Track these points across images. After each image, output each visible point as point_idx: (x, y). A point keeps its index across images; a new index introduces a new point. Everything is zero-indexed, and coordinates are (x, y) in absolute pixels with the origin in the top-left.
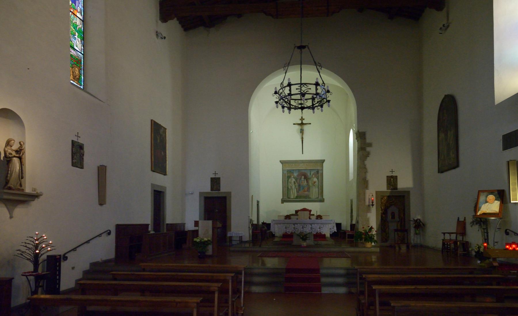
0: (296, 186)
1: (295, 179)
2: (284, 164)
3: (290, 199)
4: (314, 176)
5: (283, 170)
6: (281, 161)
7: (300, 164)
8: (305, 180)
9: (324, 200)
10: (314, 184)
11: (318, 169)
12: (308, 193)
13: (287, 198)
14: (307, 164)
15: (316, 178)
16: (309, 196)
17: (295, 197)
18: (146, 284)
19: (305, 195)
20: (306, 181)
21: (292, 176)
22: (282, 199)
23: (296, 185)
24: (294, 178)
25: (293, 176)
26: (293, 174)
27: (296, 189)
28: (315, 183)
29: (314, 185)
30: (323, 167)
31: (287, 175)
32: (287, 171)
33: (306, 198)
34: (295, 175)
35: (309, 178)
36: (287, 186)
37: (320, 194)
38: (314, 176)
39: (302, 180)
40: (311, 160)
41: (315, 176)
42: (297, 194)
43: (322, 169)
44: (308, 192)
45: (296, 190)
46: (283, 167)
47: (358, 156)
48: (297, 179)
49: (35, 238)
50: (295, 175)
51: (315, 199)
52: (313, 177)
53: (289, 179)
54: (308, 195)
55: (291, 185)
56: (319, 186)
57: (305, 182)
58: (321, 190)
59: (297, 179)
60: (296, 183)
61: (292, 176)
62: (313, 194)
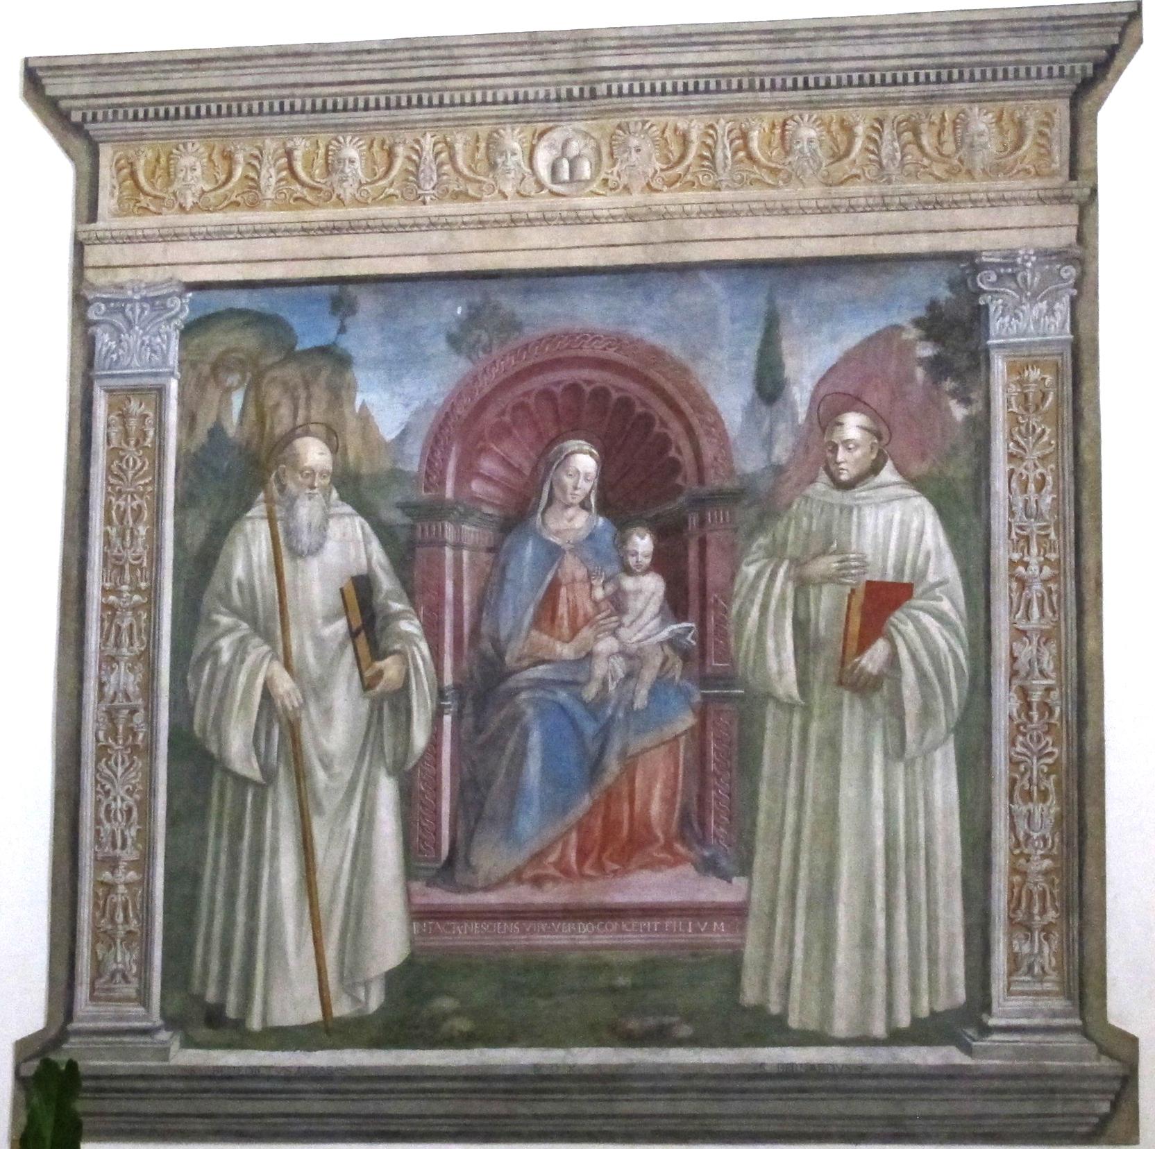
0: (400, 699)
1: (384, 532)
2: (107, 154)
3: (241, 1037)
4: (853, 425)
5: (80, 301)
6: (54, 88)
7: (514, 140)
8: (643, 544)
9: (1127, 1081)
10: (874, 658)
11: (969, 261)
12: (715, 892)
13: (172, 1022)
14: (696, 128)
15: (918, 484)
16: (733, 963)
17: (375, 1000)
18: (170, 587)
19: (635, 936)
20: (660, 563)
21: (314, 453)
22: (25, 1049)
23: (391, 668)
24: (364, 509)
25: (332, 437)
26: (339, 394)
27: (387, 791)
28: (902, 623)
29: (864, 686)
30: (1087, 206)
31: (189, 419)
32: (182, 309)
33: (660, 1037)
34: (389, 423)
35: (732, 497)
36: (182, 705)
37: (1020, 926)
38: (853, 425)
39: (554, 553)
40: (778, 34)
41: (880, 431)
42: (419, 915)
43: (1061, 256)
44: (709, 867)
45: (407, 797)
46: (107, 221)
47: (1096, 248)
48: (434, 511)
49: (959, 412)
50: (389, 423)
51: (896, 1037)
52: (848, 462)
53: (220, 532)
54: (718, 933)
55: (284, 684)
56: (1005, 703)
57: (618, 603)
58: (1046, 812)
59: (434, 511)
60: (410, 626)
61: (314, 453)
62: (825, 899)
